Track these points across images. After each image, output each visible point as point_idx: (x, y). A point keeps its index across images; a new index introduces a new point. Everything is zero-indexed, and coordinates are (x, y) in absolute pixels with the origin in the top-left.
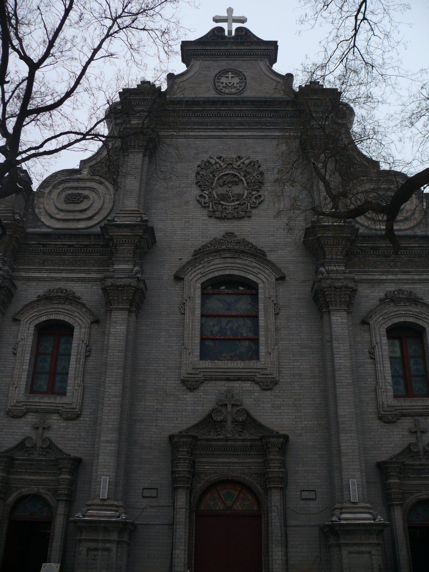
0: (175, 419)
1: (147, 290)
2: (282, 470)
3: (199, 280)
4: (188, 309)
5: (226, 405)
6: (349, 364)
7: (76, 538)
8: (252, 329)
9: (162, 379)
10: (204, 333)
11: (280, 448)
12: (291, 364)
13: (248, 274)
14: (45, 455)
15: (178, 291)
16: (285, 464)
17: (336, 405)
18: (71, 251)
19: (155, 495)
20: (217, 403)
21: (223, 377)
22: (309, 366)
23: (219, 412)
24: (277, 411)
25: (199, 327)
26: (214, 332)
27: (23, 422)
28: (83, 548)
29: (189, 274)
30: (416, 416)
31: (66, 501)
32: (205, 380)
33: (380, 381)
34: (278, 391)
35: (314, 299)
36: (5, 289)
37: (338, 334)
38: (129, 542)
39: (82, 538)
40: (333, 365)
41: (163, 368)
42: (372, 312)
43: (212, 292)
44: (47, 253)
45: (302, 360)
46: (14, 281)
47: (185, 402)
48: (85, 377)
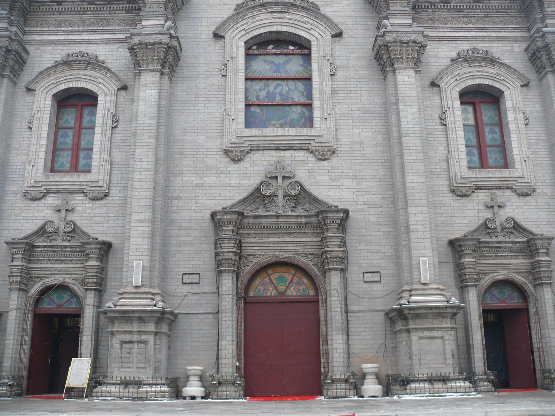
0: (218, 195)
1: (181, 51)
2: (342, 249)
3: (242, 38)
5: (276, 178)
6: (418, 129)
7: (108, 330)
8: (305, 93)
9: (201, 150)
10: (249, 98)
11: (339, 225)
12: (351, 131)
13: (299, 30)
14: (69, 240)
15: (219, 51)
16: (344, 243)
18: (92, 9)
19: (197, 281)
20: (266, 176)
21: (272, 145)
22: (371, 133)
23: (268, 186)
24: (334, 184)
25: (243, 90)
26: (261, 97)
27: (43, 205)
28: (116, 341)
29: (230, 32)
30: (492, 189)
31: (95, 290)
32: (251, 150)
33: (453, 149)
34: (335, 162)
35: (376, 58)
36: (14, 53)
37: (405, 95)
38: (168, 333)
39: (114, 330)
40: (399, 131)
41: (203, 137)
42: (443, 73)
44: (64, 12)
46: (26, 46)
47: (228, 175)
48: (112, 150)
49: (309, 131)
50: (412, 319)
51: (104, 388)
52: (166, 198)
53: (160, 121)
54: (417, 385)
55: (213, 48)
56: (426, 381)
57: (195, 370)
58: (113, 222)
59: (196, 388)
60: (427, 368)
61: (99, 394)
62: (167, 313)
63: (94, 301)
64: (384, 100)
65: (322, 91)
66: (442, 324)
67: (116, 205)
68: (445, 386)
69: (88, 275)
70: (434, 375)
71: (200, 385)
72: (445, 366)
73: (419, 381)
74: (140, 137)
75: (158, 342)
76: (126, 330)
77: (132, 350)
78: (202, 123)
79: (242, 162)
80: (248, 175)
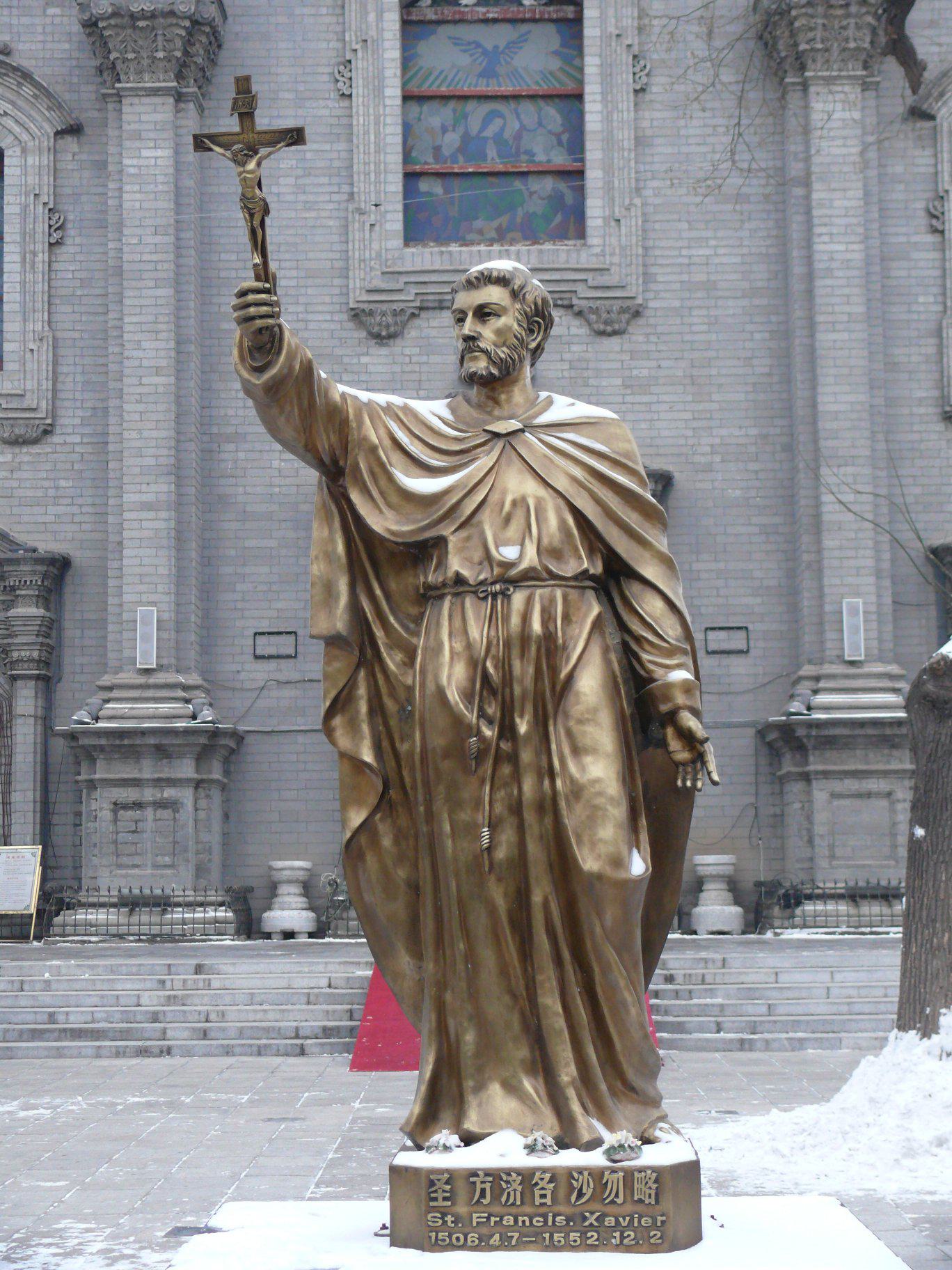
4: (361, 82)
8: (565, 137)
10: (414, 154)
12: (684, 252)
17: (813, 385)
19: (291, 651)
22: (738, 260)
24: (637, 399)
26: (446, 152)
28: (100, 804)
32: (421, 309)
34: (641, 338)
37: (828, 160)
38: (225, 780)
39: (97, 776)
40: (809, 260)
41: (294, 273)
43: (434, 17)
45: (715, 238)
49: (574, 255)
50: (815, 748)
51: (81, 916)
52: (205, 438)
53: (182, 235)
54: (820, 907)
55: (313, 11)
56: (841, 897)
57: (292, 869)
58: (69, 501)
59: (296, 912)
60: (848, 867)
61: (69, 929)
62: (225, 733)
63: (36, 707)
64: (779, 164)
65: (609, 142)
66: (888, 762)
67: (76, 457)
68: (886, 910)
69: (16, 641)
70: (862, 884)
71: (305, 906)
72: (892, 863)
73: (824, 897)
74: (134, 283)
75: (203, 803)
76: (125, 776)
77: (140, 825)
78: (292, 231)
79: (398, 341)
80: (415, 377)
